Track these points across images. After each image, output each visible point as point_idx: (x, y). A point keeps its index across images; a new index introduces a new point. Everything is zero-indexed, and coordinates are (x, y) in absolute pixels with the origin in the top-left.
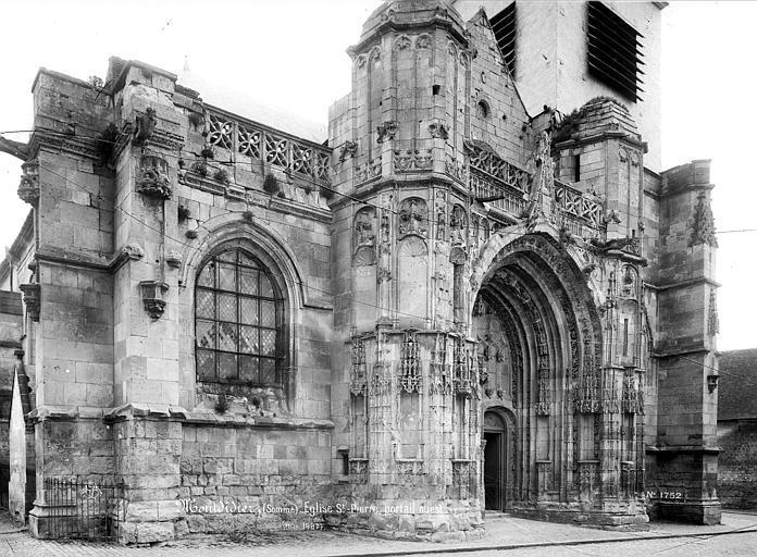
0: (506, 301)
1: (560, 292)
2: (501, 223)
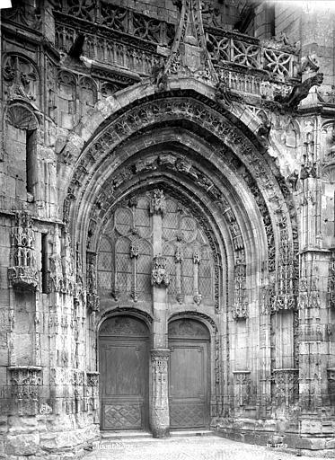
0: (191, 194)
1: (243, 170)
2: (116, 83)
